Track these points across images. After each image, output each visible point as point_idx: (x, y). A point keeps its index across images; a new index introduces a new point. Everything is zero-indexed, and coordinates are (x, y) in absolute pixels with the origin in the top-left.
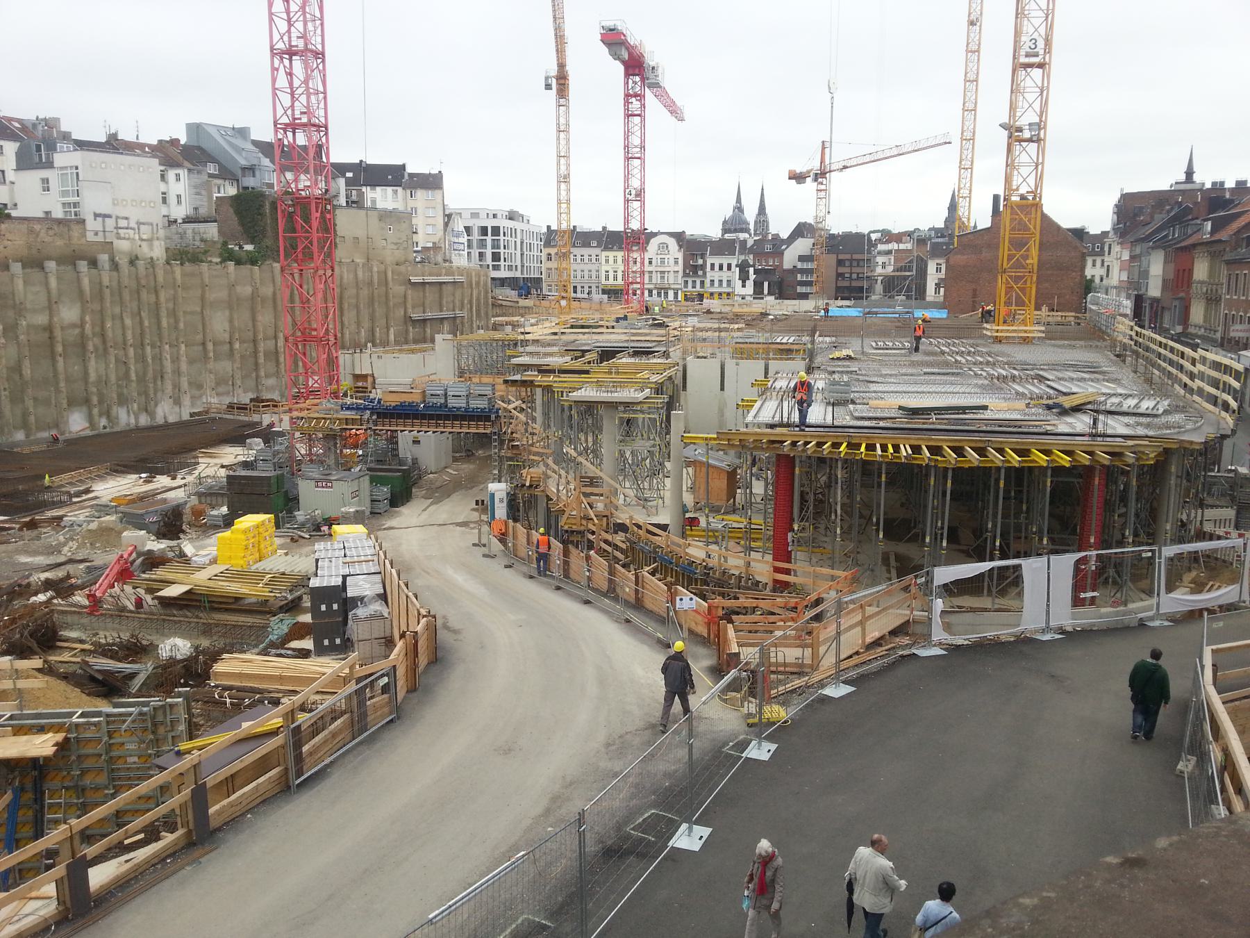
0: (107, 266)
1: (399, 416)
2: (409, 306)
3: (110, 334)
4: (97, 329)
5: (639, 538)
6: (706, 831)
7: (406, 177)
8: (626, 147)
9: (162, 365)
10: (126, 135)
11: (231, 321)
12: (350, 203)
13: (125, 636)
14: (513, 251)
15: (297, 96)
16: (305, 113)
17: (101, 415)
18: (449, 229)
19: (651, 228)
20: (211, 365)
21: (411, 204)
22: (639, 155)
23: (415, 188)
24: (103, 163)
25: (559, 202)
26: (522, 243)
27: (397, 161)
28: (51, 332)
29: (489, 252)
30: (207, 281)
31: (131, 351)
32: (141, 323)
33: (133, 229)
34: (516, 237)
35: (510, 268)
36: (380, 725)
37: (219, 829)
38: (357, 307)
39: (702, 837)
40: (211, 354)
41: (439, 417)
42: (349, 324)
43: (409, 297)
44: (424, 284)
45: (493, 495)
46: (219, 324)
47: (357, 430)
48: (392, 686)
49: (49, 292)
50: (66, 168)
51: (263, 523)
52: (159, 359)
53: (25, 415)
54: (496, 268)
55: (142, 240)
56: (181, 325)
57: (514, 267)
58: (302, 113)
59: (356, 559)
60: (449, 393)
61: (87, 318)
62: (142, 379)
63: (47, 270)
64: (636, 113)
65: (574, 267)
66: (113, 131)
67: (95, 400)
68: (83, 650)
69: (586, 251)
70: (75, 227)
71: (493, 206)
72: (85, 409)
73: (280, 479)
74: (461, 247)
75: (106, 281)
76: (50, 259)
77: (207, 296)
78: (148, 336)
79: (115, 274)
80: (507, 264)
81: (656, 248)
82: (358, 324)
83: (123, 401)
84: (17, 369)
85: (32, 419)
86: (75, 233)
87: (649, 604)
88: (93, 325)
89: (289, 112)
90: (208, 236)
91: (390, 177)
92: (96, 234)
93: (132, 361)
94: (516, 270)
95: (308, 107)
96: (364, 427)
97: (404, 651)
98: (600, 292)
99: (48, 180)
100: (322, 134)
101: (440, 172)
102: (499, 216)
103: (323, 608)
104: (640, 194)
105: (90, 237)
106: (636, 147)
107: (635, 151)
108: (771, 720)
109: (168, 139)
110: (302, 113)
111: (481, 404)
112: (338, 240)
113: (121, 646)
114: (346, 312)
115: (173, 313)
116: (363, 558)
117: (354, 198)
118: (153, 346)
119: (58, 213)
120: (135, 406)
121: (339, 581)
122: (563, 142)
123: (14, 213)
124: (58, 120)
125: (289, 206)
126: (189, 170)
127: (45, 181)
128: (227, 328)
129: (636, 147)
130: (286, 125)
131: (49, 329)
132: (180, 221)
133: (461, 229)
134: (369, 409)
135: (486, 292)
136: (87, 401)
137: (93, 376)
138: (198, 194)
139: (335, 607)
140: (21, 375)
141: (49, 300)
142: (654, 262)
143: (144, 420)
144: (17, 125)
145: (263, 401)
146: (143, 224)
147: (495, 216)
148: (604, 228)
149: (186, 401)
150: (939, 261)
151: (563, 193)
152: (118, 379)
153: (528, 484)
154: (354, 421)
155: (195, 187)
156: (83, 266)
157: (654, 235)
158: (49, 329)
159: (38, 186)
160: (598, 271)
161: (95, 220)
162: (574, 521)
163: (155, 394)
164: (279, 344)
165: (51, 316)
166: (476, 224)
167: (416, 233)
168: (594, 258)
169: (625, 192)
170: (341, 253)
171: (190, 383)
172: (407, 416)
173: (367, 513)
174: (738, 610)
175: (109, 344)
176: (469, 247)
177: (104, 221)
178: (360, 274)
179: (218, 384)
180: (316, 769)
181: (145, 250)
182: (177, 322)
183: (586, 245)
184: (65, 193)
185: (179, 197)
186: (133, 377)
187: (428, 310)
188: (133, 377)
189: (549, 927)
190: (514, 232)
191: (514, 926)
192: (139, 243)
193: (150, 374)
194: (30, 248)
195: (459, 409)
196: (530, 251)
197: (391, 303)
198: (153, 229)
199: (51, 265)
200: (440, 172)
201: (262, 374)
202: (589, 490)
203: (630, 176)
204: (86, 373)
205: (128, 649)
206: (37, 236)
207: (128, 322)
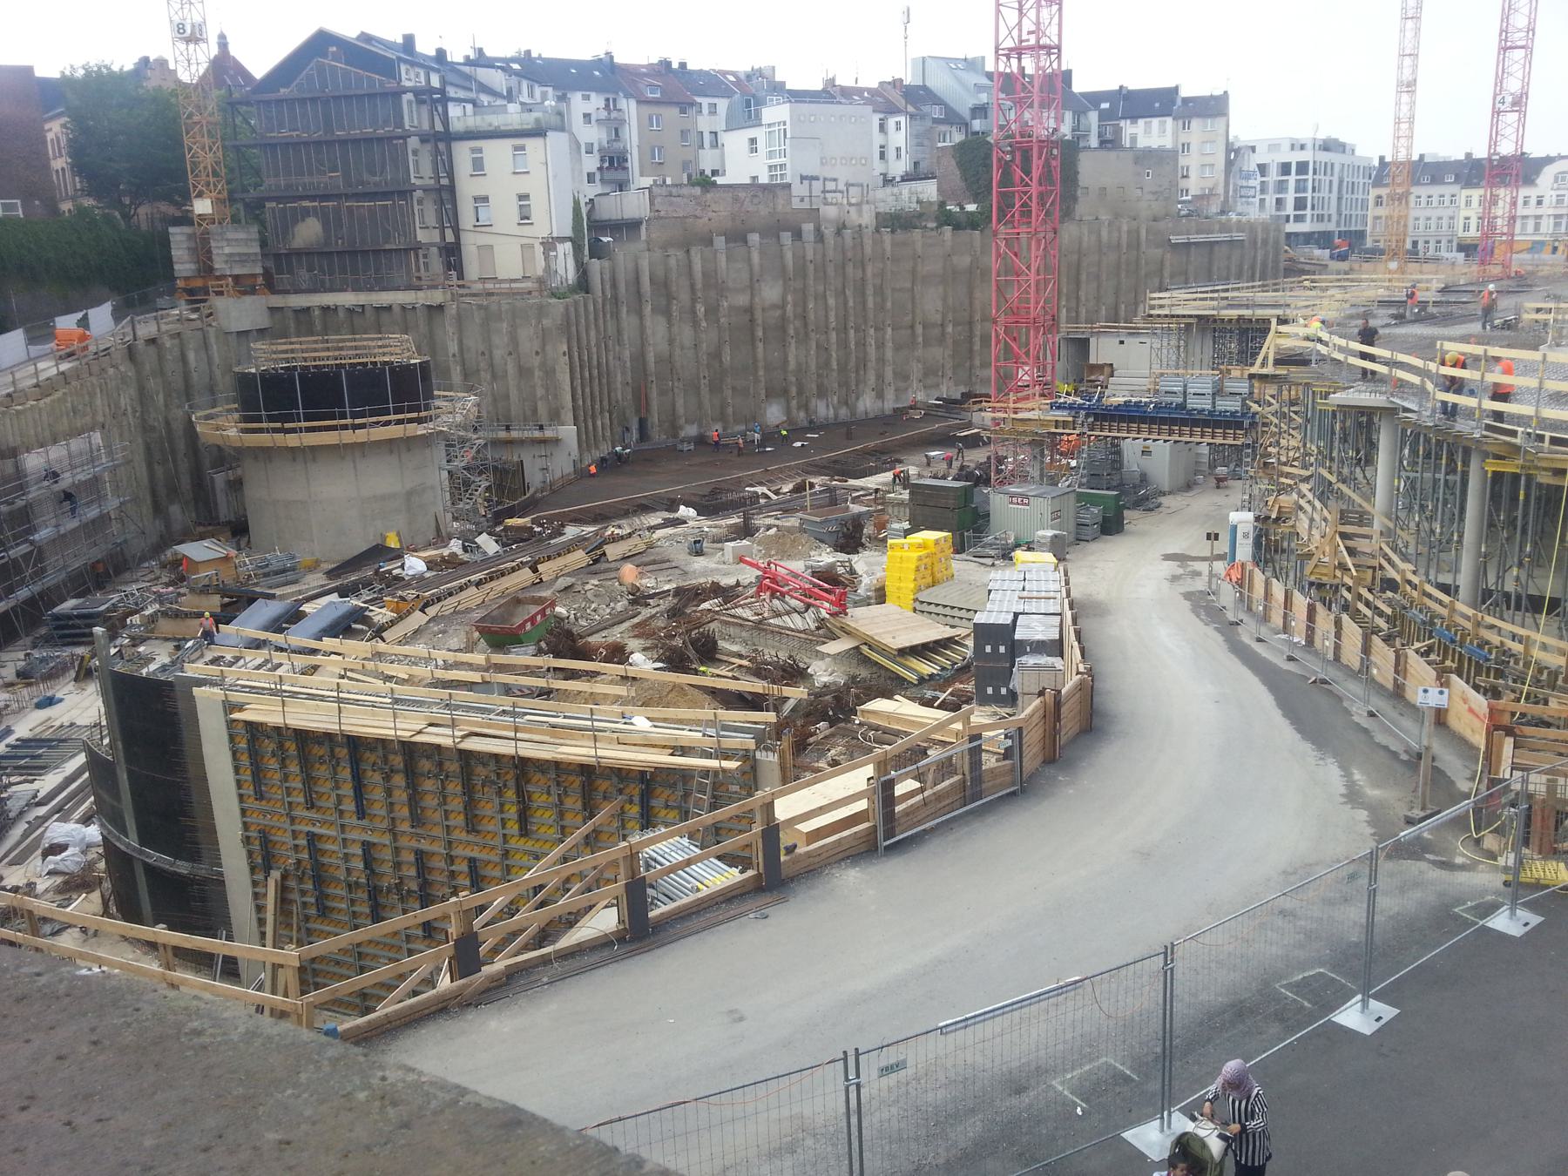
0: (812, 238)
1: (1122, 419)
2: (1166, 274)
3: (812, 316)
4: (799, 310)
5: (1412, 603)
6: (1389, 1012)
7: (1179, 102)
8: (1504, 31)
9: (865, 353)
10: (845, 80)
11: (944, 299)
12: (1104, 143)
13: (783, 656)
17: (799, 408)
18: (1235, 169)
19: (1535, 150)
20: (919, 352)
21: (1183, 138)
22: (1523, 43)
23: (1190, 117)
25: (1398, 122)
26: (1341, 182)
28: (752, 314)
29: (1290, 197)
30: (919, 251)
31: (833, 336)
32: (846, 303)
34: (1332, 175)
35: (1320, 218)
36: (1000, 794)
37: (792, 879)
38: (1098, 277)
39: (1380, 1018)
40: (920, 339)
41: (1173, 422)
42: (1087, 300)
43: (1167, 264)
44: (1188, 245)
45: (1235, 528)
46: (931, 303)
47: (1069, 435)
48: (1016, 751)
49: (751, 270)
51: (937, 542)
52: (862, 344)
53: (723, 407)
54: (1299, 219)
55: (850, 204)
56: (889, 304)
58: (1030, 33)
59: (1035, 594)
60: (1189, 390)
61: (789, 298)
62: (843, 368)
63: (750, 244)
65: (1413, 213)
66: (830, 76)
67: (794, 390)
68: (740, 666)
69: (1436, 190)
70: (780, 193)
71: (1304, 134)
72: (782, 400)
73: (967, 494)
74: (1252, 193)
75: (810, 255)
76: (753, 231)
77: (919, 268)
78: (852, 318)
79: (820, 245)
80: (1316, 212)
81: (1552, 180)
82: (1098, 299)
83: (822, 393)
84: (716, 355)
85: (730, 410)
86: (780, 202)
87: (1409, 695)
88: (795, 305)
89: (1015, 33)
90: (924, 197)
91: (1157, 105)
92: (802, 200)
93: (834, 347)
94: (1329, 220)
95: (1038, 24)
96: (1077, 432)
97: (1042, 712)
98: (1455, 248)
100: (1053, 57)
101: (1226, 92)
102: (1309, 146)
103: (988, 649)
104: (1519, 102)
105: (796, 204)
106: (1520, 30)
108: (1542, 882)
109: (890, 80)
110: (1030, 33)
111: (1229, 405)
112: (1079, 193)
113: (776, 665)
114: (1083, 286)
115: (879, 291)
116: (1043, 594)
117: (1109, 136)
118: (857, 330)
120: (835, 398)
121: (1008, 619)
122: (1410, 34)
123: (720, 180)
125: (1008, 153)
126: (912, 116)
127: (753, 141)
128: (940, 309)
129: (1520, 30)
130: (1011, 50)
131: (750, 310)
132: (898, 179)
133: (1253, 167)
134: (1084, 409)
135: (1277, 254)
136: (785, 392)
137: (792, 365)
139: (1002, 649)
140: (721, 362)
141: (751, 279)
142: (1546, 201)
143: (844, 413)
144: (732, 78)
145: (976, 396)
146: (853, 185)
147: (1302, 147)
149: (890, 394)
152: (819, 367)
153: (1274, 516)
154: (1065, 424)
155: (917, 136)
156: (786, 237)
158: (750, 310)
159: (746, 145)
160: (1452, 218)
162: (1325, 571)
163: (857, 385)
165: (752, 295)
166: (1274, 159)
167: (1186, 177)
168: (1447, 199)
169: (1494, 99)
170: (1082, 208)
171: (895, 373)
172: (1131, 420)
173: (1072, 538)
174: (1550, 720)
175: (811, 327)
176: (1263, 191)
178: (1104, 233)
179: (926, 375)
180: (910, 833)
181: (854, 218)
182: (884, 300)
183: (1436, 180)
184: (771, 154)
185: (898, 149)
186: (834, 365)
187: (1192, 279)
188: (834, 365)
189: (1133, 1080)
190: (1328, 168)
191: (1087, 1068)
193: (852, 364)
194: (733, 220)
195: (1201, 411)
197: (1143, 272)
199: (754, 238)
200: (1226, 92)
202: (1349, 529)
204: (786, 361)
205: (784, 670)
206: (742, 204)
207: (831, 302)
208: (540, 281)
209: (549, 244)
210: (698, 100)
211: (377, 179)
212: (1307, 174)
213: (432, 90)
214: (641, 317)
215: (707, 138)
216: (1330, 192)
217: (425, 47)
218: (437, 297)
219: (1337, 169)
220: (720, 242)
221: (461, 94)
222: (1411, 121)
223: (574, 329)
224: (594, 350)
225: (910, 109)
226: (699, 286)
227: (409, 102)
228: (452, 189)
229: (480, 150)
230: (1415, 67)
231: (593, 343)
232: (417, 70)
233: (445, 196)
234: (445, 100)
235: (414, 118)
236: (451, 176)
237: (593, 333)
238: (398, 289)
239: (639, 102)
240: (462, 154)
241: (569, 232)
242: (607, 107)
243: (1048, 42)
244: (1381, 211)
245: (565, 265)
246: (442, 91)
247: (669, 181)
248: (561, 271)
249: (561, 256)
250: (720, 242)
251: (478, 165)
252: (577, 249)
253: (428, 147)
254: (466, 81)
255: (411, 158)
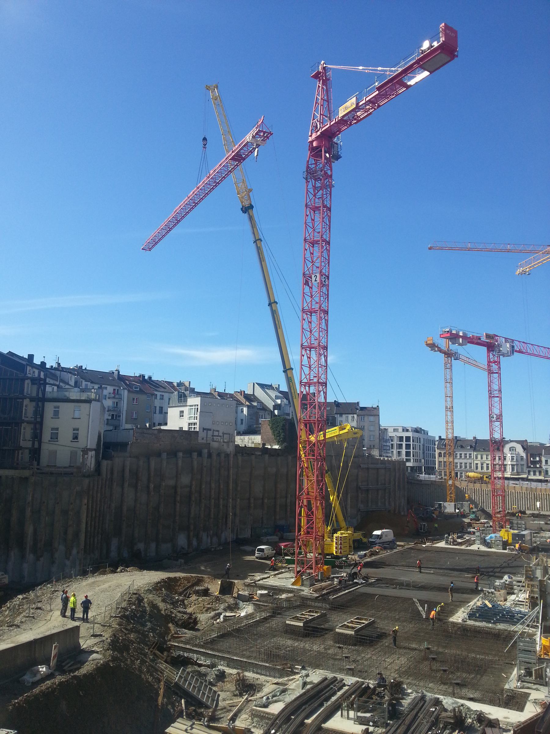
0: (206, 456)
14: (418, 451)
15: (312, 369)
16: (316, 377)
22: (498, 395)
24: (209, 403)
25: (447, 422)
26: (423, 445)
27: (355, 401)
29: (404, 451)
33: (221, 436)
34: (420, 443)
40: (252, 505)
50: (192, 406)
55: (224, 442)
56: (239, 488)
57: (419, 460)
61: (194, 483)
64: (495, 371)
67: (192, 527)
74: (388, 448)
89: (308, 377)
99: (183, 411)
101: (378, 406)
104: (499, 418)
105: (200, 440)
106: (496, 390)
107: (496, 393)
119: (186, 428)
120: (211, 532)
124: (194, 389)
127: (182, 412)
129: (496, 390)
131: (175, 488)
138: (251, 419)
146: (226, 434)
148: (475, 438)
150: (466, 453)
151: (449, 417)
156: (195, 455)
157: (507, 442)
158: (175, 488)
159: (178, 414)
161: (203, 431)
164: (288, 500)
168: (468, 455)
169: (490, 416)
177: (207, 432)
186: (212, 516)
188: (212, 516)
192: (223, 443)
196: (429, 451)
198: (230, 436)
199: (180, 454)
200: (378, 406)
201: (278, 517)
203: (493, 407)
207: (213, 485)
208: (79, 468)
209: (85, 451)
210: (156, 393)
211: (6, 416)
212: (410, 441)
213: (40, 379)
214: (123, 489)
215: (158, 409)
216: (420, 450)
217: (37, 361)
218: (26, 473)
219: (422, 440)
220: (164, 455)
221: (52, 382)
222: (452, 422)
223: (91, 493)
224: (99, 502)
225: (247, 403)
226: (152, 474)
227: (28, 384)
228: (41, 423)
229: (58, 407)
230: (452, 401)
231: (99, 499)
232: (34, 370)
233: (38, 426)
234: (45, 384)
235: (29, 389)
236: (42, 417)
237: (99, 495)
238: (6, 468)
239: (129, 391)
240: (49, 408)
241: (94, 446)
242: (114, 393)
243: (322, 381)
244: (441, 459)
245: (91, 460)
246: (45, 380)
247: (139, 427)
248: (89, 464)
249: (90, 457)
250: (164, 455)
251: (56, 414)
252: (97, 455)
253: (34, 404)
254: (54, 377)
255: (24, 408)
